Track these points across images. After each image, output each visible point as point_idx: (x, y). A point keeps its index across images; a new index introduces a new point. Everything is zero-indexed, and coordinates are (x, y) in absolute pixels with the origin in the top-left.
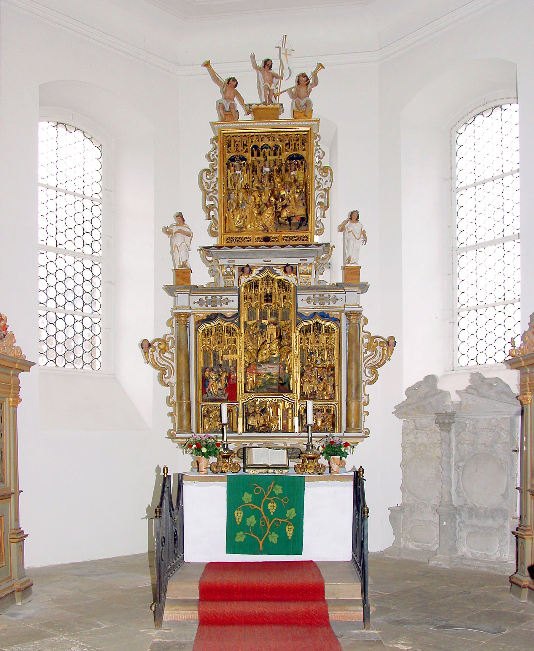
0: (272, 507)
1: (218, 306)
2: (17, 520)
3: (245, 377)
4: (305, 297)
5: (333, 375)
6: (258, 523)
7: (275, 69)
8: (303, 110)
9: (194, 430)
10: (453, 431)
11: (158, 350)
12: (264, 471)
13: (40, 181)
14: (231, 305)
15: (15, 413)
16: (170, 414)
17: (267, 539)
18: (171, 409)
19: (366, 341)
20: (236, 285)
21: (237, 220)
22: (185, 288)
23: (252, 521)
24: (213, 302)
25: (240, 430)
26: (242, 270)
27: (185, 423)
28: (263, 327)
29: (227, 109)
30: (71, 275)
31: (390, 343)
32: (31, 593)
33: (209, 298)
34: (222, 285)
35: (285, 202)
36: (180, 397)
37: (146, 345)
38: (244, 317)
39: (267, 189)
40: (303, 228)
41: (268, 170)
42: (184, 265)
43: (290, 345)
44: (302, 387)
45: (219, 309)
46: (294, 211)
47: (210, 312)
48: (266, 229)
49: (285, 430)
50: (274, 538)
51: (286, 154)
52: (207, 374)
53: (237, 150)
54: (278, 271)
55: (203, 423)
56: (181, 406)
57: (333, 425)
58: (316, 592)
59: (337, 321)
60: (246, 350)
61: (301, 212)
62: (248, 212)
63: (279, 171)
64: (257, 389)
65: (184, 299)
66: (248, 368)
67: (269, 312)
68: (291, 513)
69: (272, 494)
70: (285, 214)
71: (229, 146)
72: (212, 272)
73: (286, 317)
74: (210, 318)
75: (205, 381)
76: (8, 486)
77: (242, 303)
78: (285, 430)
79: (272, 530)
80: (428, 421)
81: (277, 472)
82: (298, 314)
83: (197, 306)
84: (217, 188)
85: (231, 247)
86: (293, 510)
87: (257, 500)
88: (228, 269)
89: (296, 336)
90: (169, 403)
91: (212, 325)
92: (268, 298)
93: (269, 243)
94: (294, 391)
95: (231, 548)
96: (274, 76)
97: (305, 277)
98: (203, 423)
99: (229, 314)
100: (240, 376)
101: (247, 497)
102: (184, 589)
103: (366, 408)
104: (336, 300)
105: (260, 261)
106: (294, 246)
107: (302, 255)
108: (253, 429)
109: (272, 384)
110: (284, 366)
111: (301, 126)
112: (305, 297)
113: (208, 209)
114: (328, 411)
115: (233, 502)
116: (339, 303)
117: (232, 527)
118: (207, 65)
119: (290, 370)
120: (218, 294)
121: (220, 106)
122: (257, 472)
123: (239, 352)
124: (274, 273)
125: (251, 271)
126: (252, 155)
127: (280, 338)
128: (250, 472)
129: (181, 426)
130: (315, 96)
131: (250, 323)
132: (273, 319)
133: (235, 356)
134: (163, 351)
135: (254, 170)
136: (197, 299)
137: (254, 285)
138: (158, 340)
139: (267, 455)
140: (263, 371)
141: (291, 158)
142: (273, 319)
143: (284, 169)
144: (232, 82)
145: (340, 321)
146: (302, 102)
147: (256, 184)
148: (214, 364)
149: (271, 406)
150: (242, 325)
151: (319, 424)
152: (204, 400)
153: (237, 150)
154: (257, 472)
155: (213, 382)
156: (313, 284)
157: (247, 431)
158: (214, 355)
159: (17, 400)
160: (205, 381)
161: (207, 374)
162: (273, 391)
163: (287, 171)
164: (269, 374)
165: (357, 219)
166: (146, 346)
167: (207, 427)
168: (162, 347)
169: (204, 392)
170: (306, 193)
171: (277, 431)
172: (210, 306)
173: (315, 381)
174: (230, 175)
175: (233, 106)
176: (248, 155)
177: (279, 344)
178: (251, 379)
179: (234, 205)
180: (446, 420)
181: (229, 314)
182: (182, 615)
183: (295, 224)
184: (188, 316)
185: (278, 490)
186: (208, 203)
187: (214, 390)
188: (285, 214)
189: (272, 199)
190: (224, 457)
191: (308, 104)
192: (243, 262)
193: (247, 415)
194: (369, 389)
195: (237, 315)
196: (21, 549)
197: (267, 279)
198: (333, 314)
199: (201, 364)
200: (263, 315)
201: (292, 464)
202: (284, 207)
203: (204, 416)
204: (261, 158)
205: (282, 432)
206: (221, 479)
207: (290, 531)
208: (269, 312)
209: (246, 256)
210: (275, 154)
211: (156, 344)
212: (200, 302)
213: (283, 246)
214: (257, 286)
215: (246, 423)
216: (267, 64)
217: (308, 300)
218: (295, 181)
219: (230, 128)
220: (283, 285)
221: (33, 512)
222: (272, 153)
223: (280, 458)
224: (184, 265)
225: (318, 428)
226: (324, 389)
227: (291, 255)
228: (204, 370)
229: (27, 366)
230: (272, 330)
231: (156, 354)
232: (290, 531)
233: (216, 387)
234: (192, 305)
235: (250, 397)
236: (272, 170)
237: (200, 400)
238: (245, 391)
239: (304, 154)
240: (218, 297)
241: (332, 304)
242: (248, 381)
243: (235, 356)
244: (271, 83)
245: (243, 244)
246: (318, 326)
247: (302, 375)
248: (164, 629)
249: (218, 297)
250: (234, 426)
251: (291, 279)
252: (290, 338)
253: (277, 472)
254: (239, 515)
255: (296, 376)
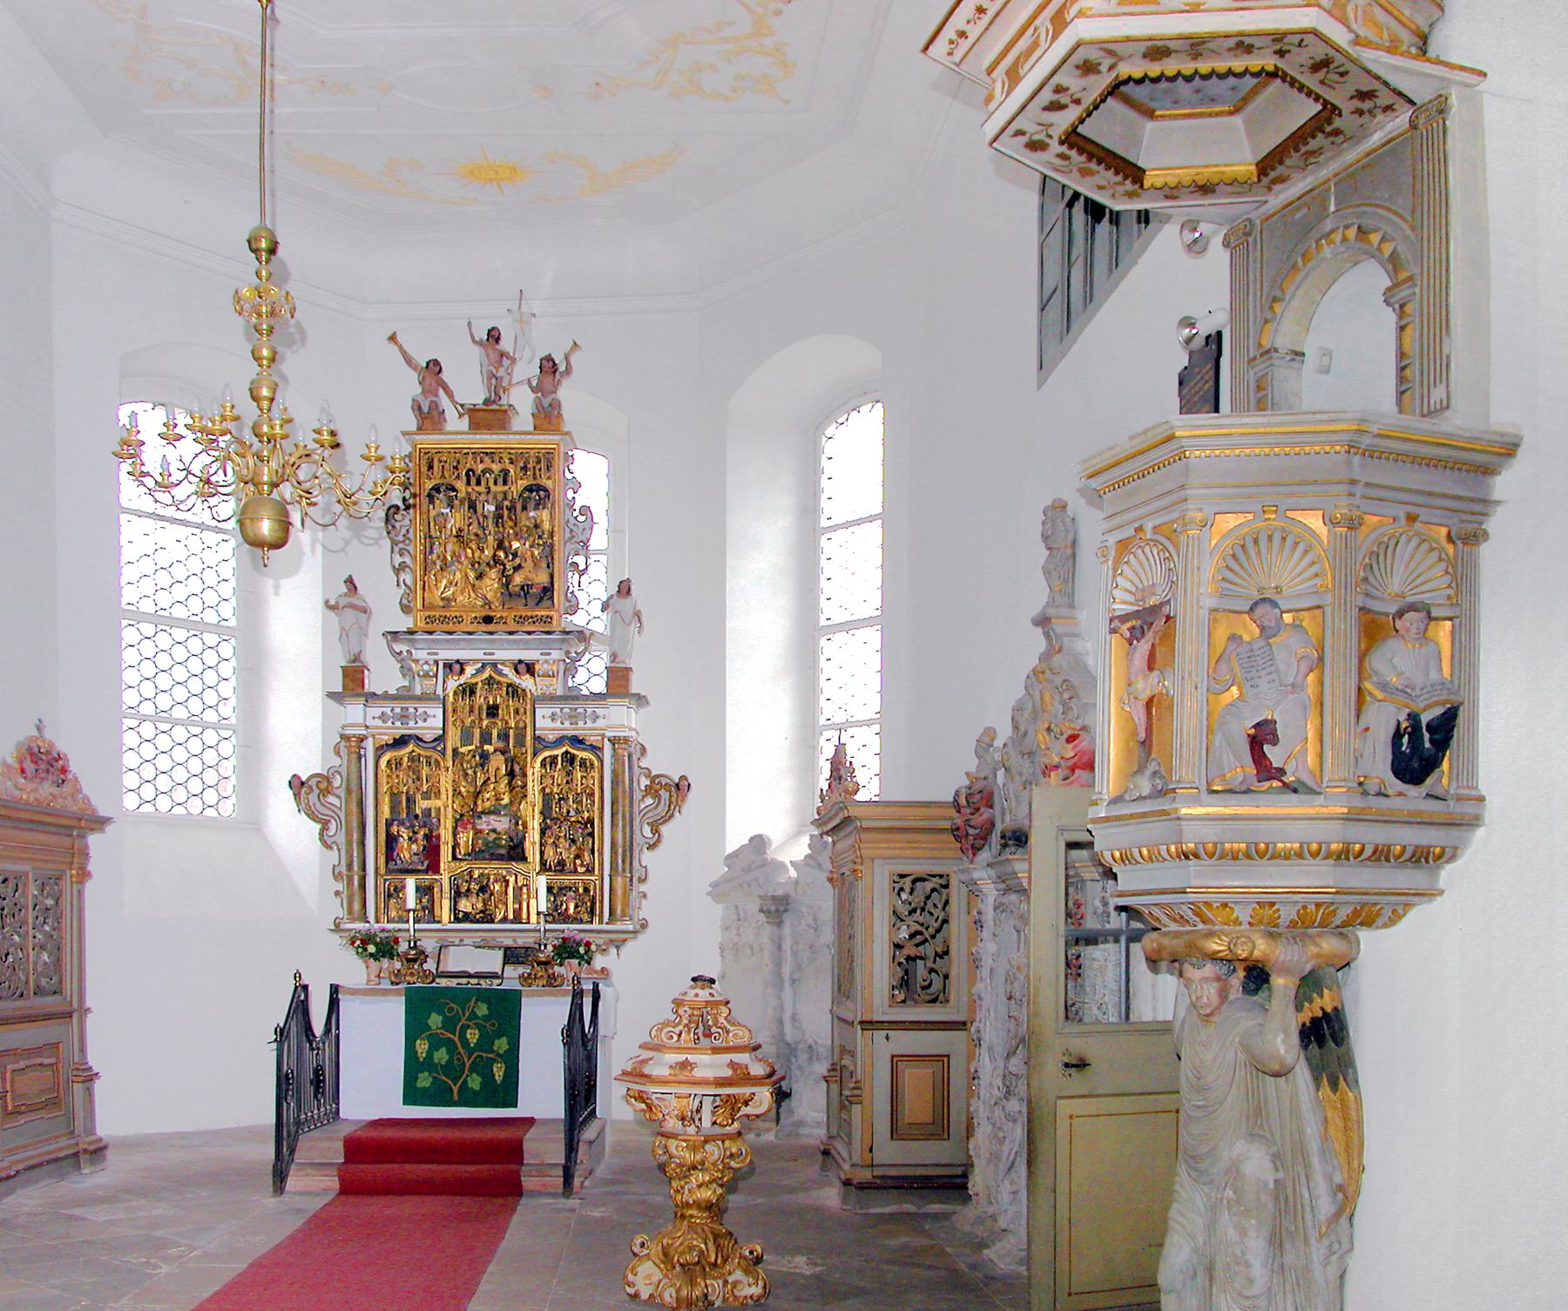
0: (473, 1036)
1: (412, 724)
2: (83, 1050)
3: (455, 835)
4: (548, 712)
5: (592, 835)
6: (451, 1058)
7: (506, 344)
8: (548, 416)
9: (371, 918)
10: (787, 924)
11: (317, 791)
12: (464, 981)
13: (124, 503)
14: (431, 722)
15: (80, 893)
16: (337, 893)
17: (465, 1082)
18: (340, 886)
19: (645, 782)
20: (440, 691)
21: (441, 588)
22: (358, 695)
23: (441, 1056)
24: (404, 717)
25: (445, 918)
26: (448, 666)
27: (357, 907)
28: (485, 757)
29: (425, 409)
30: (134, 746)
31: (680, 788)
32: (104, 1157)
33: (398, 710)
34: (418, 692)
35: (518, 561)
36: (350, 866)
37: (297, 783)
38: (453, 739)
39: (490, 539)
40: (546, 603)
41: (492, 508)
42: (357, 659)
43: (525, 786)
44: (542, 853)
45: (412, 728)
46: (531, 576)
47: (398, 733)
48: (488, 603)
49: (517, 919)
50: (475, 1082)
51: (522, 483)
52: (394, 829)
53: (443, 476)
54: (506, 671)
55: (387, 907)
56: (351, 876)
57: (592, 912)
58: (513, 1152)
59: (596, 749)
60: (457, 792)
61: (542, 578)
62: (458, 576)
63: (511, 509)
64: (475, 855)
65: (355, 712)
66: (459, 822)
67: (495, 733)
68: (502, 1044)
69: (474, 1015)
70: (518, 579)
71: (431, 467)
72: (406, 670)
73: (520, 742)
74: (401, 742)
75: (391, 840)
76: (1360, 539)
77: (451, 720)
78: (517, 913)
79: (472, 1070)
80: (753, 906)
81: (485, 984)
82: (537, 739)
83: (379, 723)
84: (411, 535)
85: (430, 633)
86: (504, 1040)
87: (449, 1024)
88: (426, 667)
89: (534, 770)
90: (337, 876)
91: (404, 752)
92: (493, 711)
93: (491, 627)
94: (530, 859)
95: (412, 1095)
96: (502, 355)
97: (547, 681)
98: (387, 907)
99: (429, 736)
100: (445, 834)
101: (435, 1020)
102: (322, 1148)
103: (642, 888)
104: (596, 717)
105: (478, 654)
106: (529, 633)
107: (545, 647)
108: (467, 918)
109: (500, 847)
110: (516, 819)
111: (545, 440)
112: (548, 712)
113: (398, 570)
114: (586, 890)
115: (415, 1027)
116: (600, 723)
117: (413, 1065)
118: (393, 338)
119: (525, 826)
120: (411, 707)
121: (417, 407)
122: (453, 983)
123: (443, 796)
124: (500, 673)
125: (462, 671)
126: (468, 483)
127: (511, 774)
128: (444, 982)
129: (350, 911)
130: (568, 394)
131: (463, 750)
132: (501, 745)
133: (438, 803)
134: (326, 792)
135: (472, 506)
136: (378, 712)
137: (469, 690)
138: (317, 775)
139: (471, 958)
140: (484, 826)
141: (530, 489)
142: (501, 745)
143: (519, 507)
144: (434, 367)
145: (601, 749)
146: (546, 403)
147: (474, 528)
148: (405, 811)
149: (496, 881)
150: (449, 753)
151: (571, 911)
152: (389, 871)
153: (443, 476)
154: (453, 983)
155: (403, 842)
156: (559, 693)
157: (457, 920)
158: (408, 800)
159: (84, 875)
160: (391, 840)
161: (394, 829)
162: (501, 858)
163: (524, 508)
164: (494, 831)
165: (629, 591)
166: (297, 785)
167: (393, 914)
168: (324, 785)
169: (389, 857)
170: (552, 546)
171: (505, 920)
172: (398, 724)
173: (563, 843)
174: (433, 513)
175: (434, 406)
176: (460, 485)
177: (510, 783)
178: (465, 838)
179: (439, 564)
180: (778, 908)
181: (429, 736)
182: (313, 1185)
183: (534, 595)
184: (362, 739)
185: (482, 1010)
186: (398, 560)
187: (405, 855)
188: (518, 579)
189: (502, 554)
190: (409, 960)
191: (555, 405)
192: (453, 655)
193: (457, 895)
194: (647, 858)
195: (441, 739)
196: (89, 1093)
197: (489, 682)
198: (593, 740)
199: (386, 812)
200: (485, 738)
201: (510, 971)
202: (517, 568)
203: (390, 896)
204: (482, 489)
205: (512, 922)
206: (397, 993)
207: (499, 1072)
208: (495, 733)
209: (455, 644)
210: (505, 483)
211: (313, 782)
212: (383, 716)
213: (511, 633)
214: (472, 693)
215: (455, 910)
216: (494, 336)
217: (553, 717)
218: (536, 526)
219: (429, 440)
220: (514, 691)
221: (107, 1039)
222: (500, 481)
223: (492, 961)
224: (357, 659)
225: (569, 916)
226: (577, 857)
227: (526, 646)
228: (389, 824)
229: (100, 823)
230: (498, 763)
231: (313, 797)
232: (499, 1072)
233: (408, 850)
234: (370, 722)
235: (464, 866)
236: (499, 508)
237: (382, 870)
238: (454, 858)
239: (549, 484)
240: (412, 710)
241: (590, 724)
242: (461, 842)
243: (438, 803)
244: (499, 364)
245: (450, 627)
246: (570, 759)
247: (543, 832)
248: (285, 1198)
249: (412, 710)
250: (437, 912)
251: (526, 682)
252: (525, 775)
253: (485, 984)
254: (422, 1047)
255: (533, 836)
